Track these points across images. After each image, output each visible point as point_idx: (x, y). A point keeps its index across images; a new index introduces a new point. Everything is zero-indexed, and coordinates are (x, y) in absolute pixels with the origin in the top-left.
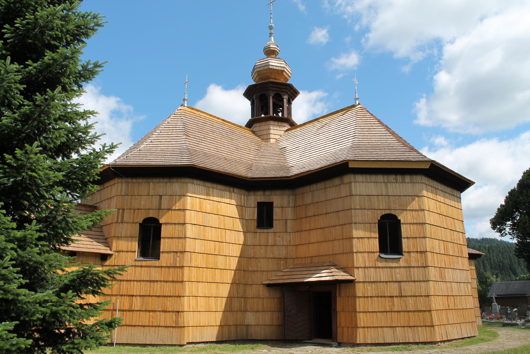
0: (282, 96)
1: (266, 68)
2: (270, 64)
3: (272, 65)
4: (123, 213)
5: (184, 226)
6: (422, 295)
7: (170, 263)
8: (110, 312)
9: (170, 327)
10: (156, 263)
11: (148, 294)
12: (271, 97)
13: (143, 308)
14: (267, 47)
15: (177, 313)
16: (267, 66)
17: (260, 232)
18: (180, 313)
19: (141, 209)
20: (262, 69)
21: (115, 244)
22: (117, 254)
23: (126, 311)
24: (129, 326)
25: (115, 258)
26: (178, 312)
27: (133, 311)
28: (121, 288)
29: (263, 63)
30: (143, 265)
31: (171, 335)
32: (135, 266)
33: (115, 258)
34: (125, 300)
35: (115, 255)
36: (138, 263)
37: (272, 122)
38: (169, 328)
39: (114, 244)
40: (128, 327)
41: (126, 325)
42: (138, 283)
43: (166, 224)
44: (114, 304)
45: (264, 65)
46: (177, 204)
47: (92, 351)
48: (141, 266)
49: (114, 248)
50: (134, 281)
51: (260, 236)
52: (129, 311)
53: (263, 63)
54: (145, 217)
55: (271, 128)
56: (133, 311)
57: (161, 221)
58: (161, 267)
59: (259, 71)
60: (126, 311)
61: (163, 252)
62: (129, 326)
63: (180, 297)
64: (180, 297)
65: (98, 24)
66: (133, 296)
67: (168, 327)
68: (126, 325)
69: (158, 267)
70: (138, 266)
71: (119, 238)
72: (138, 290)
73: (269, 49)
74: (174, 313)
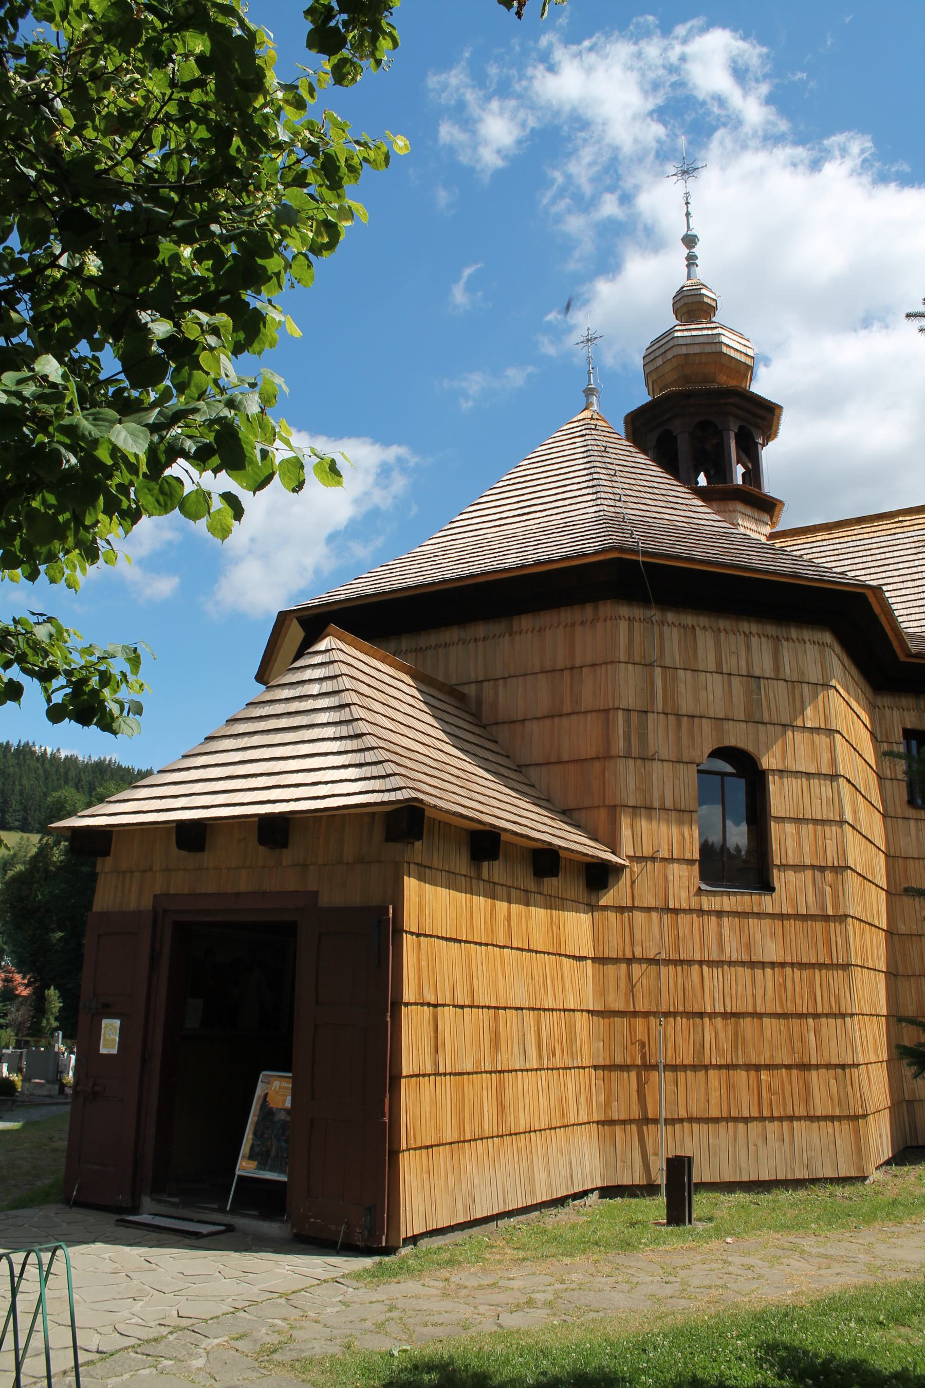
0: (755, 436)
1: (708, 349)
2: (724, 339)
3: (728, 346)
4: (644, 726)
5: (835, 784)
6: (820, 1010)
7: (807, 903)
8: (633, 1074)
9: (826, 1118)
10: (767, 903)
11: (750, 1010)
12: (732, 434)
13: (737, 1058)
14: (693, 292)
15: (839, 1071)
16: (713, 346)
17: (916, 819)
18: (847, 1071)
19: (701, 717)
20: (696, 350)
21: (629, 833)
22: (636, 868)
23: (684, 1068)
24: (699, 1120)
25: (633, 883)
26: (843, 1067)
27: (706, 1068)
28: (664, 988)
29: (699, 333)
30: (727, 908)
31: (832, 1147)
32: (701, 912)
33: (633, 883)
34: (678, 1028)
35: (632, 872)
36: (710, 902)
37: (740, 507)
38: (822, 1124)
39: (626, 833)
40: (695, 1126)
41: (691, 1120)
42: (715, 970)
43: (781, 772)
44: (643, 1045)
45: (702, 340)
46: (809, 711)
47: (877, 1225)
48: (719, 914)
49: (627, 848)
50: (701, 963)
51: (918, 830)
52: (694, 1068)
53: (699, 333)
54: (715, 747)
55: (740, 522)
56: (706, 1068)
57: (768, 762)
58: (782, 917)
59: (687, 355)
60: (684, 1068)
61: (784, 867)
62: (699, 1120)
63: (843, 1016)
64: (843, 1016)
65: (578, 58)
66: (701, 1015)
67: (818, 1119)
68: (691, 1120)
69: (772, 916)
70: (709, 913)
71: (645, 809)
72: (716, 996)
73: (698, 299)
74: (832, 1072)
